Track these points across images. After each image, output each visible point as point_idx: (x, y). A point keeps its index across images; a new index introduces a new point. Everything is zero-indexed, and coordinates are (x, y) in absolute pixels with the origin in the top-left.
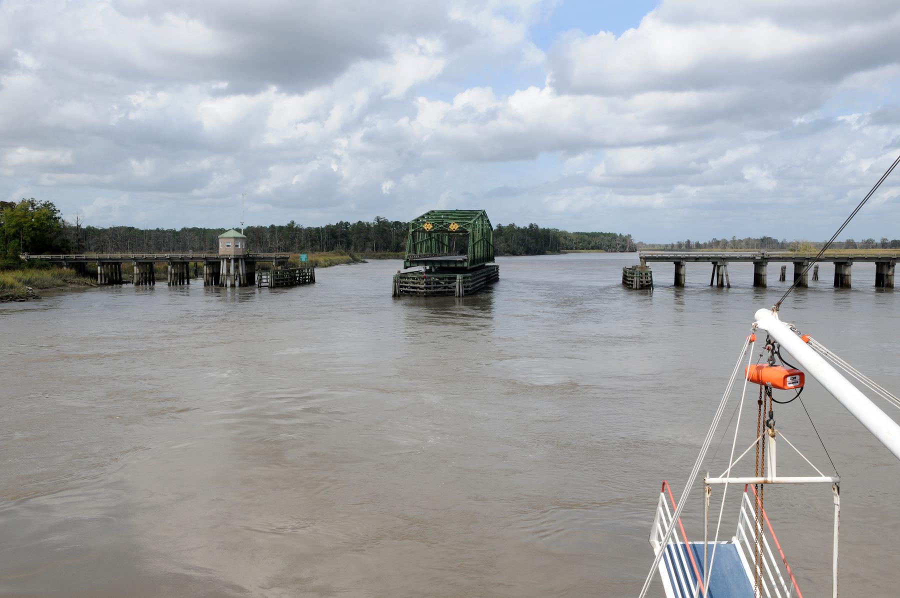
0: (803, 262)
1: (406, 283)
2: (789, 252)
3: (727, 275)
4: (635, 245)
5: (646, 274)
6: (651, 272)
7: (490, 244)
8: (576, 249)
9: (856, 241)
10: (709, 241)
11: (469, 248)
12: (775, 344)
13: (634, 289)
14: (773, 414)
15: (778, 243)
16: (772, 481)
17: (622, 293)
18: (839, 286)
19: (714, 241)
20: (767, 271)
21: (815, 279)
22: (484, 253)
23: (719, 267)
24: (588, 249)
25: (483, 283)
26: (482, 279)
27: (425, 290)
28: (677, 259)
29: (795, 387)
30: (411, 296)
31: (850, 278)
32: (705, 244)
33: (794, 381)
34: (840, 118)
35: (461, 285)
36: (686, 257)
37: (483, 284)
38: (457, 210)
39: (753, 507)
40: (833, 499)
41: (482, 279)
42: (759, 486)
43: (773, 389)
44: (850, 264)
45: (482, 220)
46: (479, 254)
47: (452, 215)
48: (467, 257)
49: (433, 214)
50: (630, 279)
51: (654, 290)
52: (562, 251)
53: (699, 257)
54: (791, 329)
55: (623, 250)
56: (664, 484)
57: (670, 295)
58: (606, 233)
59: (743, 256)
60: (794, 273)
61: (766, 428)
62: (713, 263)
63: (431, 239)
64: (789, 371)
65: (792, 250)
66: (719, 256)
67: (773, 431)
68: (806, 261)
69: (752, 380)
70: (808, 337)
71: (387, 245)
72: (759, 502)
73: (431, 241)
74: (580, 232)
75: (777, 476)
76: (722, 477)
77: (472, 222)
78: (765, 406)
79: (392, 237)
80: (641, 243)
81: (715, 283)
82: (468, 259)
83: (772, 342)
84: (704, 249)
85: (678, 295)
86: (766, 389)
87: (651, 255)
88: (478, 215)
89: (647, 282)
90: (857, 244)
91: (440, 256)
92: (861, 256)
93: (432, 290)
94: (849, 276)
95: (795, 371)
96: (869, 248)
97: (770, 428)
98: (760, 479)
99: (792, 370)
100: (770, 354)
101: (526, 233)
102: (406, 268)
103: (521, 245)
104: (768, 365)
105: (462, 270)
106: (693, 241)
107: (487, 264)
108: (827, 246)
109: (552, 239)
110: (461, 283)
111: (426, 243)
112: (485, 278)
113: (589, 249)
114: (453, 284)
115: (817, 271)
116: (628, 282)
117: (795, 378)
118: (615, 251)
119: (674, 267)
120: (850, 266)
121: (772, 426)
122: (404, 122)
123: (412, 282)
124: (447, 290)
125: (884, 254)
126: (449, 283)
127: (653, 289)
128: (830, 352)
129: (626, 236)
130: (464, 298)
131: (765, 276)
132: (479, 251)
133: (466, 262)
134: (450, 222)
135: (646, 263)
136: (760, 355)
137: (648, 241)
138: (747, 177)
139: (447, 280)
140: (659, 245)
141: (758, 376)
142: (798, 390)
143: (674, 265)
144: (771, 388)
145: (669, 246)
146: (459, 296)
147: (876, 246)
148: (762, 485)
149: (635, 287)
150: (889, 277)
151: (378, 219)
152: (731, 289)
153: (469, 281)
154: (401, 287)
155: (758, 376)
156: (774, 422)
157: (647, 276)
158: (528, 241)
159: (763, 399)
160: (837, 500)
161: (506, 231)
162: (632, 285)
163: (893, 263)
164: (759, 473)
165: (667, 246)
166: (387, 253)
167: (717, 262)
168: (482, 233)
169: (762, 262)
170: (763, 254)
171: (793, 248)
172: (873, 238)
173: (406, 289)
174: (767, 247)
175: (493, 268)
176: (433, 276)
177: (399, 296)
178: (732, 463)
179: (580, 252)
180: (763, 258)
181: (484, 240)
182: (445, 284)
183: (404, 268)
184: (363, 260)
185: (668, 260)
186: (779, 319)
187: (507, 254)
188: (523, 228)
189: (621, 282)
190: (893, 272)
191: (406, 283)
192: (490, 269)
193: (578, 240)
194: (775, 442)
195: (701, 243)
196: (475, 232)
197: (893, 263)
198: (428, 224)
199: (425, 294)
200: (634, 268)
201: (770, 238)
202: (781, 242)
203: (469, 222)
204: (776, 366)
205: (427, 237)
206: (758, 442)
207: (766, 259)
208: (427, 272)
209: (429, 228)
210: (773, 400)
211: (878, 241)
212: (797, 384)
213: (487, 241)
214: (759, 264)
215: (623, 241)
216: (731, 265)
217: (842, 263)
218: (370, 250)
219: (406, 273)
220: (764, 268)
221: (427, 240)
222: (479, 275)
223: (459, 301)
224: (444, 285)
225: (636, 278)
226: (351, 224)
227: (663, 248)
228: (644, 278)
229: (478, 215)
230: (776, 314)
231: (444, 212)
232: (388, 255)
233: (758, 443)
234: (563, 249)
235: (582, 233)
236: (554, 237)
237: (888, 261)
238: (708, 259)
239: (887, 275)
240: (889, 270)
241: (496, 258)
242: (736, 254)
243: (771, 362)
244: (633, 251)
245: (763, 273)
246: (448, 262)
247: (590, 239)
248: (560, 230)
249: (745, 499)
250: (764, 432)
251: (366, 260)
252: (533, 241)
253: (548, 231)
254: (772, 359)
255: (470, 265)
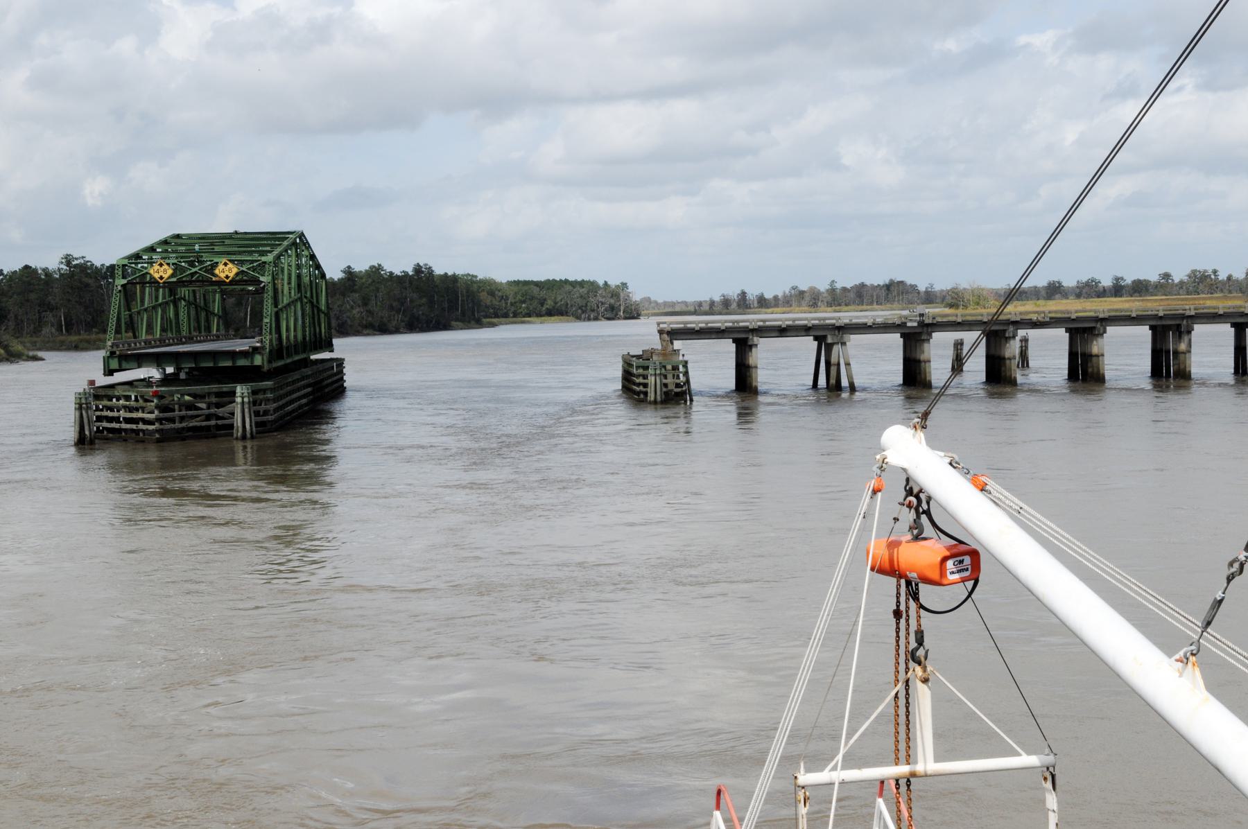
0: (1004, 331)
1: (111, 409)
2: (947, 311)
3: (848, 364)
4: (637, 304)
5: (675, 368)
6: (686, 362)
7: (319, 310)
8: (515, 315)
9: (1065, 284)
10: (785, 293)
11: (266, 320)
12: (921, 495)
13: (650, 403)
14: (922, 637)
15: (919, 293)
16: (925, 772)
17: (620, 412)
18: (1078, 379)
19: (793, 292)
20: (932, 352)
21: (1023, 366)
22: (304, 331)
23: (829, 348)
24: (539, 315)
25: (304, 401)
26: (302, 392)
27: (157, 426)
28: (739, 332)
29: (963, 580)
30: (125, 440)
31: (1103, 361)
32: (776, 298)
33: (961, 567)
34: (1023, 40)
35: (246, 410)
36: (760, 327)
37: (306, 405)
38: (236, 233)
39: (892, 818)
40: (1043, 801)
41: (302, 392)
42: (903, 782)
43: (921, 585)
44: (1101, 332)
45: (298, 256)
46: (292, 334)
47: (223, 244)
48: (261, 341)
49: (179, 241)
50: (641, 380)
51: (694, 403)
52: (485, 320)
53: (788, 326)
54: (951, 464)
55: (612, 316)
56: (719, 792)
57: (729, 413)
58: (576, 282)
59: (879, 320)
60: (985, 355)
61: (912, 664)
62: (816, 338)
63: (175, 303)
64: (949, 548)
65: (951, 306)
66: (828, 322)
67: (925, 669)
68: (1011, 328)
69: (880, 570)
70: (983, 479)
71: (93, 318)
72: (903, 807)
73: (176, 307)
74: (522, 279)
75: (938, 758)
76: (830, 771)
77: (269, 258)
78: (907, 621)
79: (104, 300)
80: (648, 300)
81: (822, 381)
82: (263, 348)
83: (915, 491)
84: (776, 310)
85: (745, 415)
86: (907, 587)
87: (682, 326)
88: (286, 243)
89: (678, 385)
90: (967, 297)
91: (200, 342)
92: (1150, 313)
93: (178, 425)
94: (1101, 358)
95: (962, 548)
96: (1092, 297)
97: (919, 663)
98: (903, 769)
99: (956, 544)
100: (913, 515)
101: (407, 284)
102: (109, 372)
103: (398, 311)
104: (909, 537)
105: (249, 374)
106: (752, 293)
107: (313, 357)
108: (1013, 294)
109: (462, 295)
110: (246, 406)
111: (164, 312)
112: (309, 389)
113: (541, 316)
114: (228, 408)
115: (1026, 347)
116: (635, 387)
117: (961, 562)
118: (596, 319)
119: (734, 349)
120: (1102, 335)
121: (923, 659)
122: (126, 46)
123: (125, 407)
124: (213, 422)
125: (1116, 310)
126: (218, 406)
127: (691, 400)
128: (1025, 507)
129: (617, 287)
130: (256, 443)
131: (927, 364)
132: (293, 328)
133: (259, 353)
134: (216, 260)
135: (672, 343)
136: (895, 519)
137: (660, 296)
138: (847, 160)
139: (214, 400)
140: (682, 302)
141: (891, 561)
142: (970, 584)
143: (734, 345)
144: (917, 585)
145: (704, 304)
146: (244, 437)
147: (1103, 293)
148: (908, 780)
149: (652, 399)
150: (1182, 356)
151: (68, 260)
152: (857, 393)
153: (268, 400)
154: (99, 419)
155: (891, 561)
156: (927, 652)
157: (676, 373)
158: (412, 301)
159: (903, 608)
160: (1052, 801)
161: (364, 280)
162: (646, 394)
163: (1188, 326)
164: (902, 754)
165: (700, 304)
166: (93, 337)
167: (825, 337)
168: (299, 286)
169: (921, 333)
170: (922, 315)
171: (954, 301)
172: (1097, 277)
173: (115, 425)
174: (899, 300)
175: (327, 365)
176: (177, 392)
177: (92, 442)
178: (849, 736)
179: (523, 322)
180: (922, 324)
181: (305, 300)
182: (208, 408)
183: (105, 375)
184: (31, 353)
185: (720, 335)
186: (927, 445)
187: (367, 332)
188: (399, 274)
189: (620, 386)
190: (1190, 345)
191: (111, 409)
192: (320, 367)
193: (519, 297)
194: (929, 692)
195: (769, 295)
196: (278, 282)
197: (1188, 326)
198: (161, 265)
199: (157, 436)
200: (646, 356)
201: (902, 282)
202: (924, 290)
203: (264, 259)
204: (925, 539)
205: (164, 298)
206: (897, 694)
207: (928, 325)
208: (167, 380)
209: (166, 276)
210: (922, 607)
211: (1107, 282)
212: (967, 574)
213: (312, 303)
214: (914, 338)
215: (612, 297)
216: (854, 340)
217: (1085, 330)
218: (53, 330)
219: (112, 386)
220: (926, 345)
221: (167, 303)
222: (294, 382)
223: (245, 447)
224: (206, 412)
225: (653, 378)
226: (5, 273)
227: (692, 309)
228: (670, 376)
229: (286, 243)
230: (921, 435)
231: (203, 238)
232: (95, 341)
233: (896, 696)
234: (486, 317)
235: (526, 283)
236: (467, 292)
237: (1178, 322)
238: (805, 330)
239: (1176, 353)
240: (1180, 342)
241: (335, 341)
242: (866, 317)
243: (915, 532)
244: (633, 318)
245: (922, 357)
246: (214, 355)
247: (543, 293)
248: (481, 276)
249: (881, 812)
250: (907, 673)
251: (40, 354)
252: (424, 300)
253: (454, 279)
254: (917, 525)
255: (270, 362)
